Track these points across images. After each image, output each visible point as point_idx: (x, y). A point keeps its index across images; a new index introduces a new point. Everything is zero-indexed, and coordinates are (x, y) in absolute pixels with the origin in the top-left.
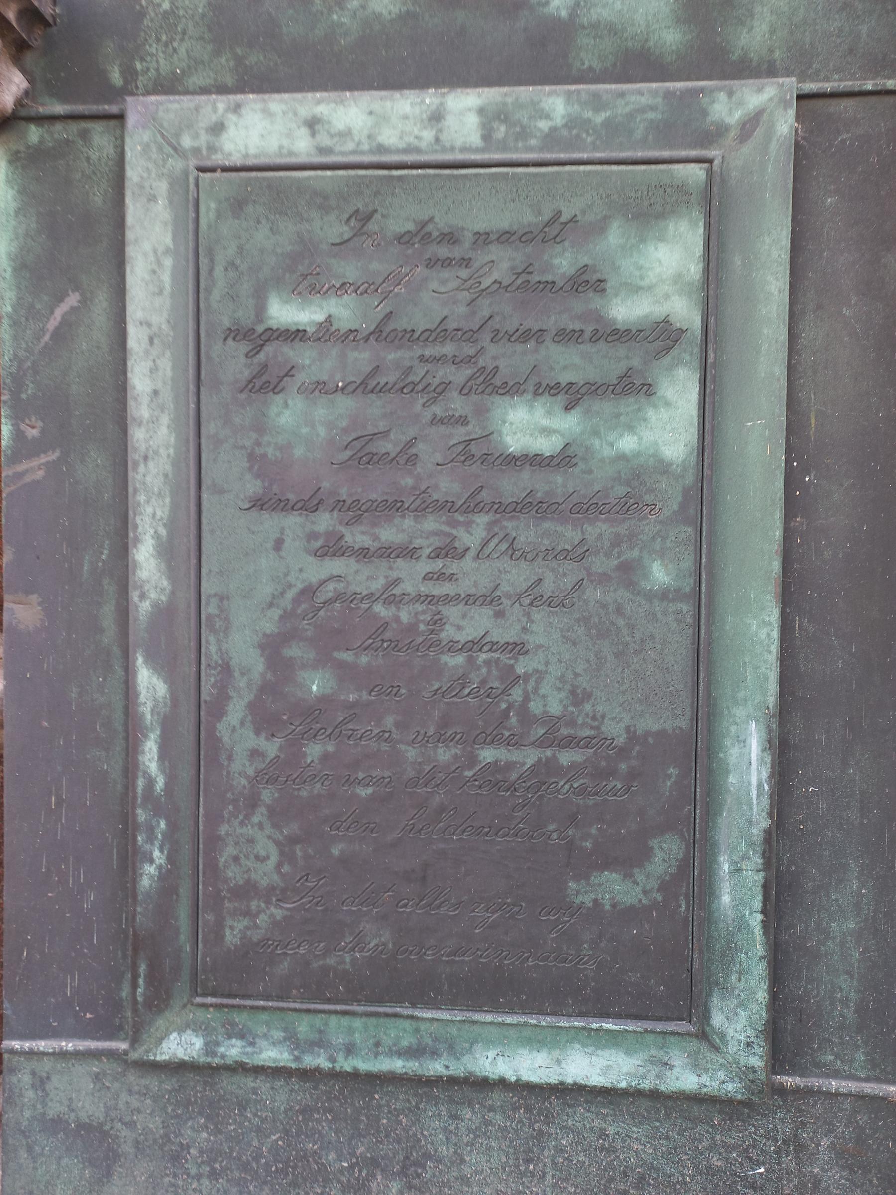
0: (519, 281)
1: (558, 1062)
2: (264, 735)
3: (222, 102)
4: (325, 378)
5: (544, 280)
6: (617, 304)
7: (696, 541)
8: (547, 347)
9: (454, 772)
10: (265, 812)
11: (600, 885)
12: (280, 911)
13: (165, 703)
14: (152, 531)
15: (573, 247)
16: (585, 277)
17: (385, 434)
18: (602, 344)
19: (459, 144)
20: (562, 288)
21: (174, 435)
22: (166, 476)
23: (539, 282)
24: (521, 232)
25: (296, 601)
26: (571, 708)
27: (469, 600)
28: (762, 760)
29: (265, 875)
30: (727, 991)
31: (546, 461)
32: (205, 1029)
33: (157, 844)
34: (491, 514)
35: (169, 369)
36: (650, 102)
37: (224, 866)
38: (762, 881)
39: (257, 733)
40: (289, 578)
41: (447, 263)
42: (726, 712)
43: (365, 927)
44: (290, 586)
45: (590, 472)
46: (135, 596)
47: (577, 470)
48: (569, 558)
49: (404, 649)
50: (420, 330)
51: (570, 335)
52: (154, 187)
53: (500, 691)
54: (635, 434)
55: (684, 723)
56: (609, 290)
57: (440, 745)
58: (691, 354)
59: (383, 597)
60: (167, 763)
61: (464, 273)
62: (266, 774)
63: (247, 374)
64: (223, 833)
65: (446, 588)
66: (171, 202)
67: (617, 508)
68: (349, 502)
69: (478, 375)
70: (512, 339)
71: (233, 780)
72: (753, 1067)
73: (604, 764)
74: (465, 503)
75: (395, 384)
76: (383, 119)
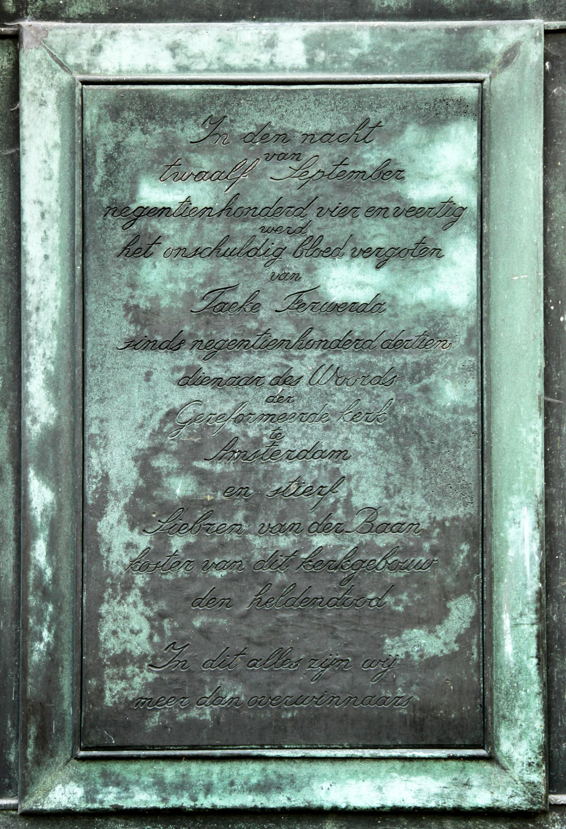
0: (338, 171)
1: (380, 789)
2: (137, 530)
3: (101, 28)
4: (186, 245)
5: (357, 170)
6: (413, 188)
7: (478, 368)
8: (360, 221)
9: (292, 555)
10: (139, 594)
11: (410, 640)
12: (151, 674)
13: (53, 509)
14: (43, 368)
15: (379, 145)
16: (389, 168)
17: (233, 288)
18: (402, 218)
19: (288, 65)
20: (371, 176)
21: (61, 290)
22: (54, 323)
23: (353, 172)
24: (338, 134)
25: (163, 422)
26: (385, 501)
27: (302, 417)
28: (533, 536)
29: (139, 645)
30: (513, 722)
31: (362, 307)
32: (86, 780)
33: (46, 625)
34: (319, 350)
35: (57, 238)
36: (434, 36)
37: (105, 640)
38: (536, 632)
39: (132, 528)
40: (157, 403)
41: (282, 157)
42: (505, 500)
43: (221, 684)
44: (158, 409)
45: (396, 315)
46: (28, 421)
47: (385, 314)
48: (381, 383)
49: (251, 458)
50: (261, 207)
51: (378, 212)
52: (44, 94)
53: (328, 489)
54: (429, 286)
55: (472, 509)
56: (407, 178)
57: (281, 534)
58: (470, 226)
59: (233, 416)
60: (54, 558)
61: (295, 165)
62: (139, 562)
63: (123, 242)
64: (103, 611)
65: (288, 408)
66: (59, 107)
67: (418, 343)
68: (205, 342)
69: (307, 242)
70: (334, 214)
71: (112, 568)
72: (533, 783)
73: (411, 544)
74: (298, 341)
75: (242, 249)
76: (229, 45)
